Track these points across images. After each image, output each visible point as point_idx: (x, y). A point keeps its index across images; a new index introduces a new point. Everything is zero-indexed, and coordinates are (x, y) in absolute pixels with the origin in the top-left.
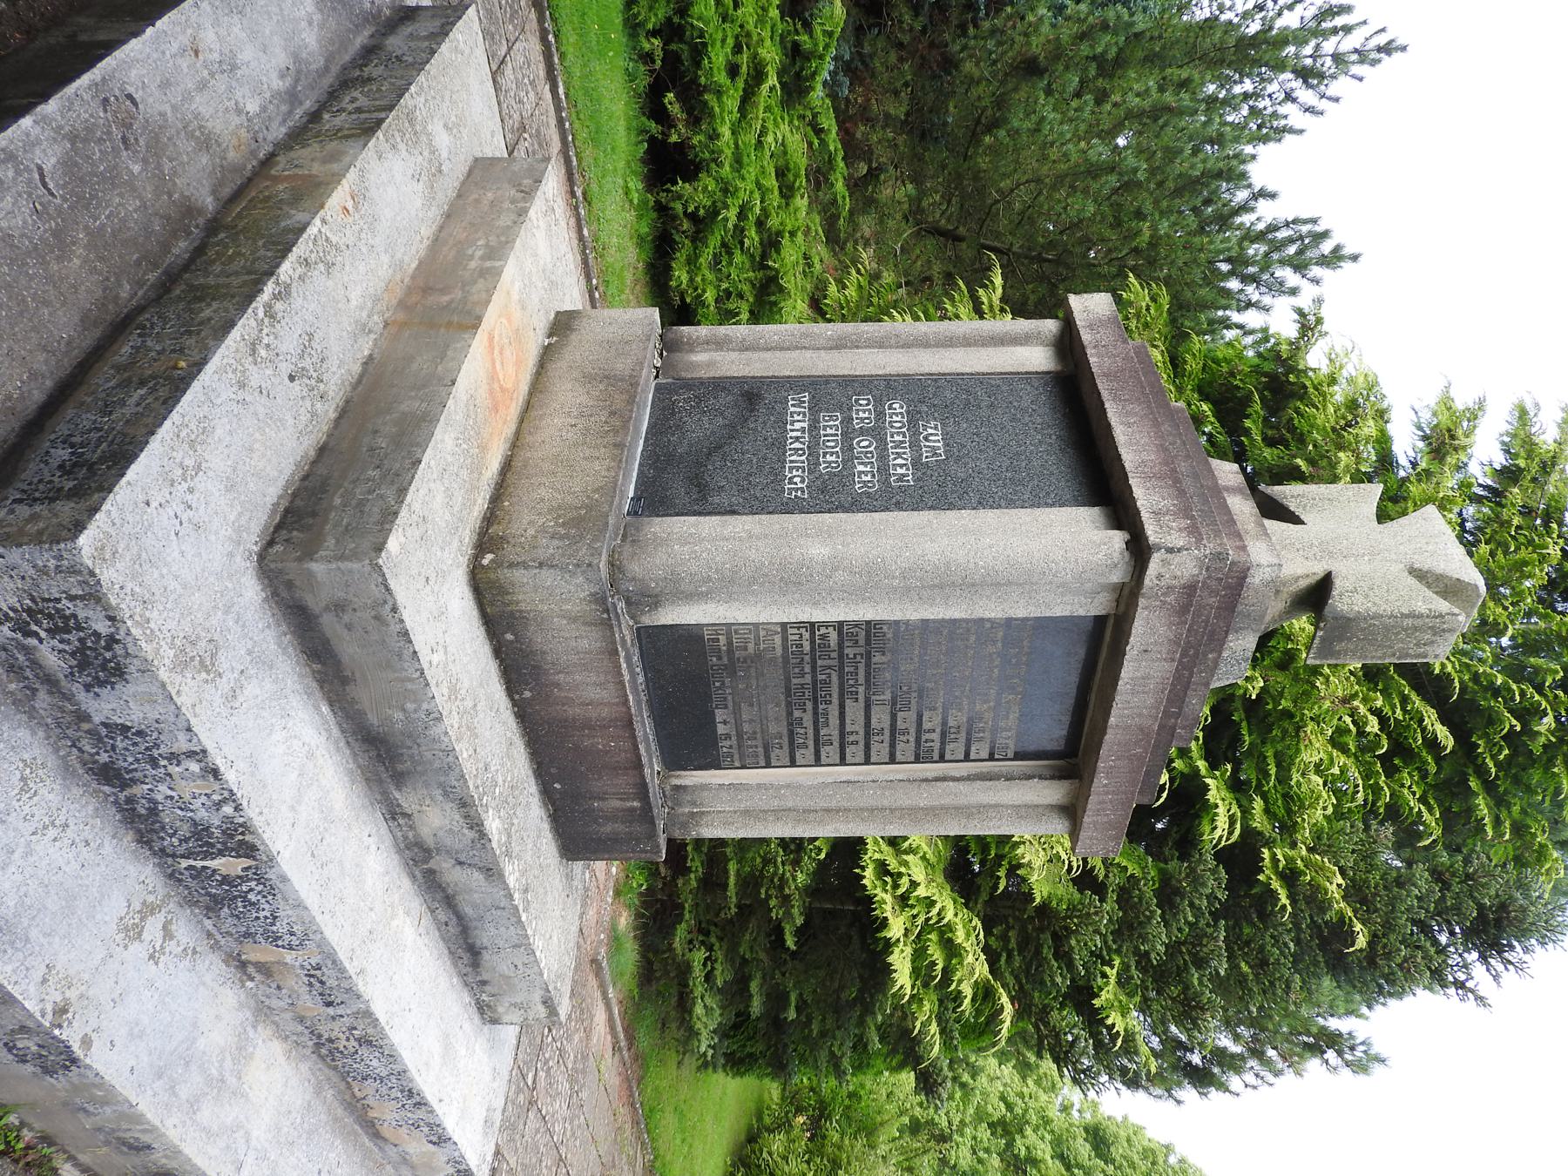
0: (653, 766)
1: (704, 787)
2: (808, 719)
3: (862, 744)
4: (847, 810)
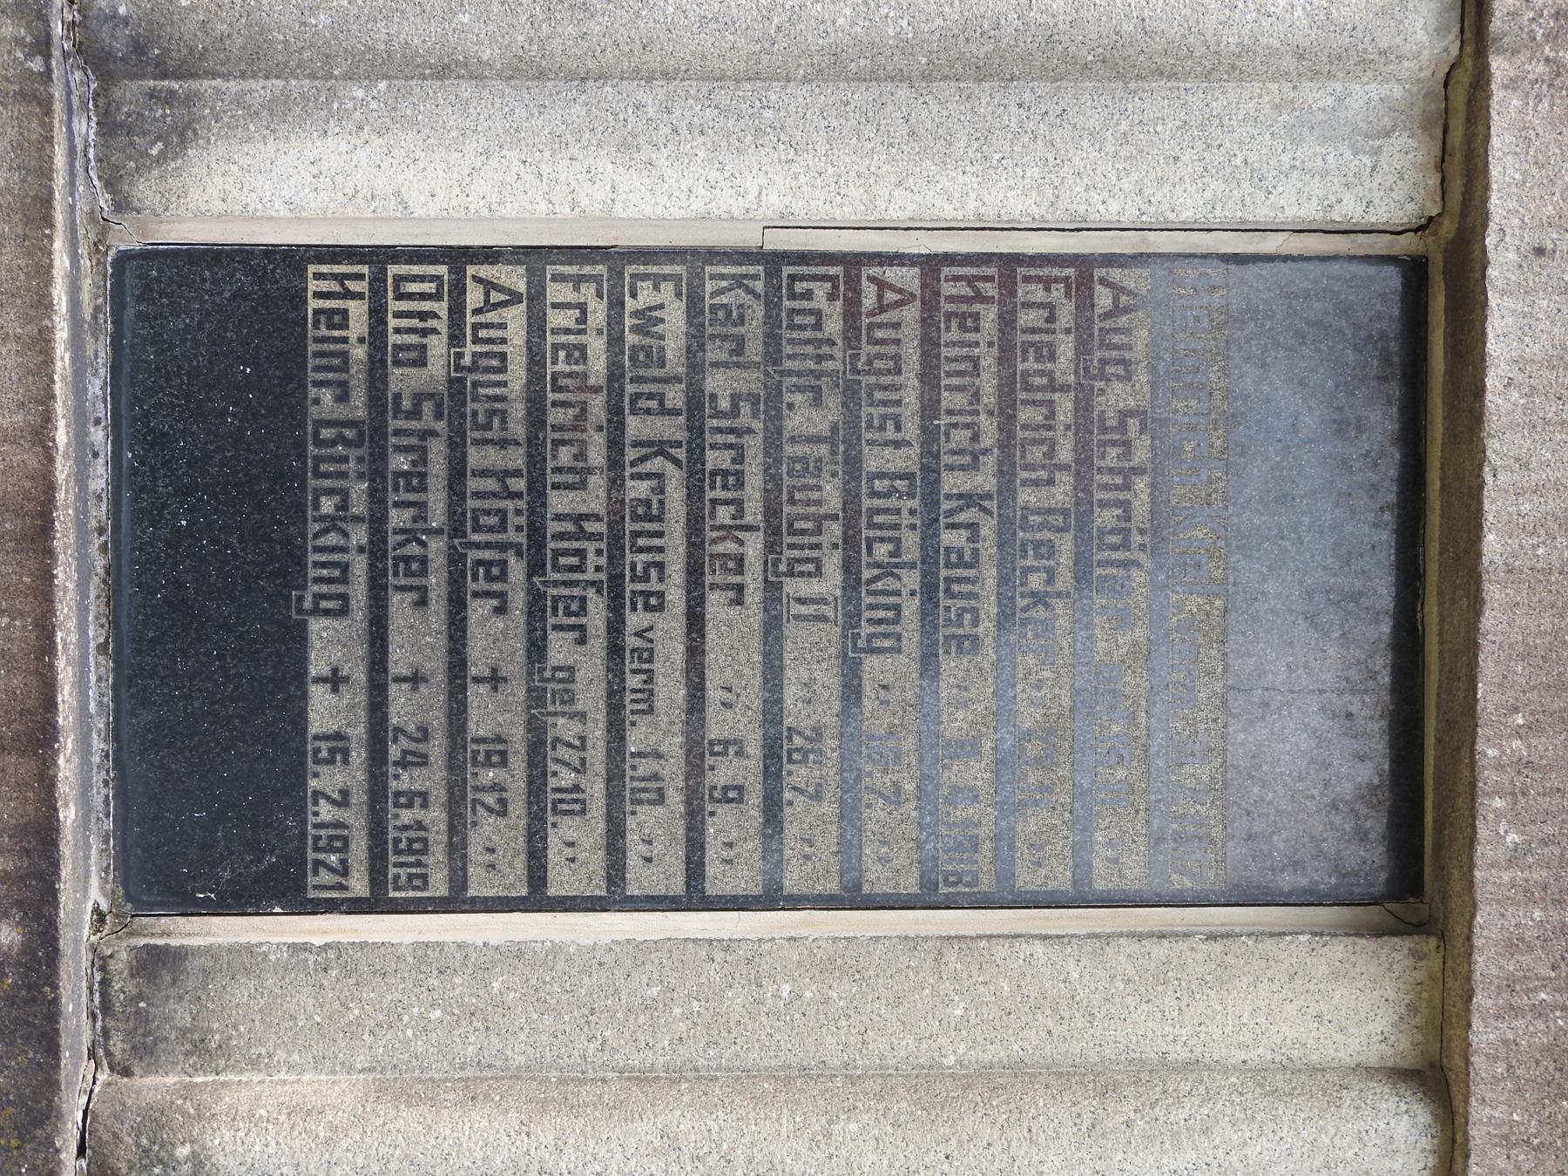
0: (85, 887)
1: (246, 959)
2: (590, 666)
3: (755, 798)
4: (702, 1077)
